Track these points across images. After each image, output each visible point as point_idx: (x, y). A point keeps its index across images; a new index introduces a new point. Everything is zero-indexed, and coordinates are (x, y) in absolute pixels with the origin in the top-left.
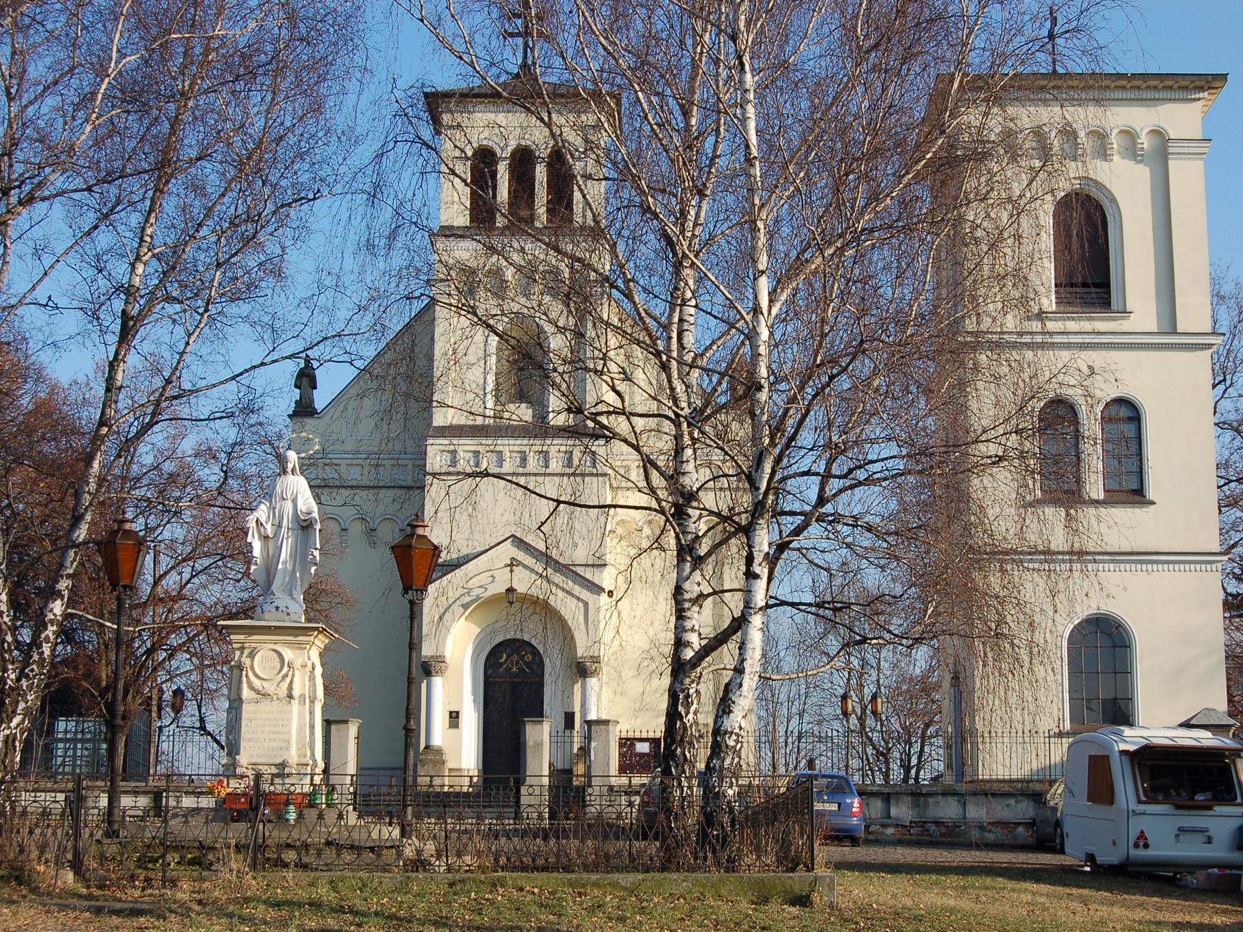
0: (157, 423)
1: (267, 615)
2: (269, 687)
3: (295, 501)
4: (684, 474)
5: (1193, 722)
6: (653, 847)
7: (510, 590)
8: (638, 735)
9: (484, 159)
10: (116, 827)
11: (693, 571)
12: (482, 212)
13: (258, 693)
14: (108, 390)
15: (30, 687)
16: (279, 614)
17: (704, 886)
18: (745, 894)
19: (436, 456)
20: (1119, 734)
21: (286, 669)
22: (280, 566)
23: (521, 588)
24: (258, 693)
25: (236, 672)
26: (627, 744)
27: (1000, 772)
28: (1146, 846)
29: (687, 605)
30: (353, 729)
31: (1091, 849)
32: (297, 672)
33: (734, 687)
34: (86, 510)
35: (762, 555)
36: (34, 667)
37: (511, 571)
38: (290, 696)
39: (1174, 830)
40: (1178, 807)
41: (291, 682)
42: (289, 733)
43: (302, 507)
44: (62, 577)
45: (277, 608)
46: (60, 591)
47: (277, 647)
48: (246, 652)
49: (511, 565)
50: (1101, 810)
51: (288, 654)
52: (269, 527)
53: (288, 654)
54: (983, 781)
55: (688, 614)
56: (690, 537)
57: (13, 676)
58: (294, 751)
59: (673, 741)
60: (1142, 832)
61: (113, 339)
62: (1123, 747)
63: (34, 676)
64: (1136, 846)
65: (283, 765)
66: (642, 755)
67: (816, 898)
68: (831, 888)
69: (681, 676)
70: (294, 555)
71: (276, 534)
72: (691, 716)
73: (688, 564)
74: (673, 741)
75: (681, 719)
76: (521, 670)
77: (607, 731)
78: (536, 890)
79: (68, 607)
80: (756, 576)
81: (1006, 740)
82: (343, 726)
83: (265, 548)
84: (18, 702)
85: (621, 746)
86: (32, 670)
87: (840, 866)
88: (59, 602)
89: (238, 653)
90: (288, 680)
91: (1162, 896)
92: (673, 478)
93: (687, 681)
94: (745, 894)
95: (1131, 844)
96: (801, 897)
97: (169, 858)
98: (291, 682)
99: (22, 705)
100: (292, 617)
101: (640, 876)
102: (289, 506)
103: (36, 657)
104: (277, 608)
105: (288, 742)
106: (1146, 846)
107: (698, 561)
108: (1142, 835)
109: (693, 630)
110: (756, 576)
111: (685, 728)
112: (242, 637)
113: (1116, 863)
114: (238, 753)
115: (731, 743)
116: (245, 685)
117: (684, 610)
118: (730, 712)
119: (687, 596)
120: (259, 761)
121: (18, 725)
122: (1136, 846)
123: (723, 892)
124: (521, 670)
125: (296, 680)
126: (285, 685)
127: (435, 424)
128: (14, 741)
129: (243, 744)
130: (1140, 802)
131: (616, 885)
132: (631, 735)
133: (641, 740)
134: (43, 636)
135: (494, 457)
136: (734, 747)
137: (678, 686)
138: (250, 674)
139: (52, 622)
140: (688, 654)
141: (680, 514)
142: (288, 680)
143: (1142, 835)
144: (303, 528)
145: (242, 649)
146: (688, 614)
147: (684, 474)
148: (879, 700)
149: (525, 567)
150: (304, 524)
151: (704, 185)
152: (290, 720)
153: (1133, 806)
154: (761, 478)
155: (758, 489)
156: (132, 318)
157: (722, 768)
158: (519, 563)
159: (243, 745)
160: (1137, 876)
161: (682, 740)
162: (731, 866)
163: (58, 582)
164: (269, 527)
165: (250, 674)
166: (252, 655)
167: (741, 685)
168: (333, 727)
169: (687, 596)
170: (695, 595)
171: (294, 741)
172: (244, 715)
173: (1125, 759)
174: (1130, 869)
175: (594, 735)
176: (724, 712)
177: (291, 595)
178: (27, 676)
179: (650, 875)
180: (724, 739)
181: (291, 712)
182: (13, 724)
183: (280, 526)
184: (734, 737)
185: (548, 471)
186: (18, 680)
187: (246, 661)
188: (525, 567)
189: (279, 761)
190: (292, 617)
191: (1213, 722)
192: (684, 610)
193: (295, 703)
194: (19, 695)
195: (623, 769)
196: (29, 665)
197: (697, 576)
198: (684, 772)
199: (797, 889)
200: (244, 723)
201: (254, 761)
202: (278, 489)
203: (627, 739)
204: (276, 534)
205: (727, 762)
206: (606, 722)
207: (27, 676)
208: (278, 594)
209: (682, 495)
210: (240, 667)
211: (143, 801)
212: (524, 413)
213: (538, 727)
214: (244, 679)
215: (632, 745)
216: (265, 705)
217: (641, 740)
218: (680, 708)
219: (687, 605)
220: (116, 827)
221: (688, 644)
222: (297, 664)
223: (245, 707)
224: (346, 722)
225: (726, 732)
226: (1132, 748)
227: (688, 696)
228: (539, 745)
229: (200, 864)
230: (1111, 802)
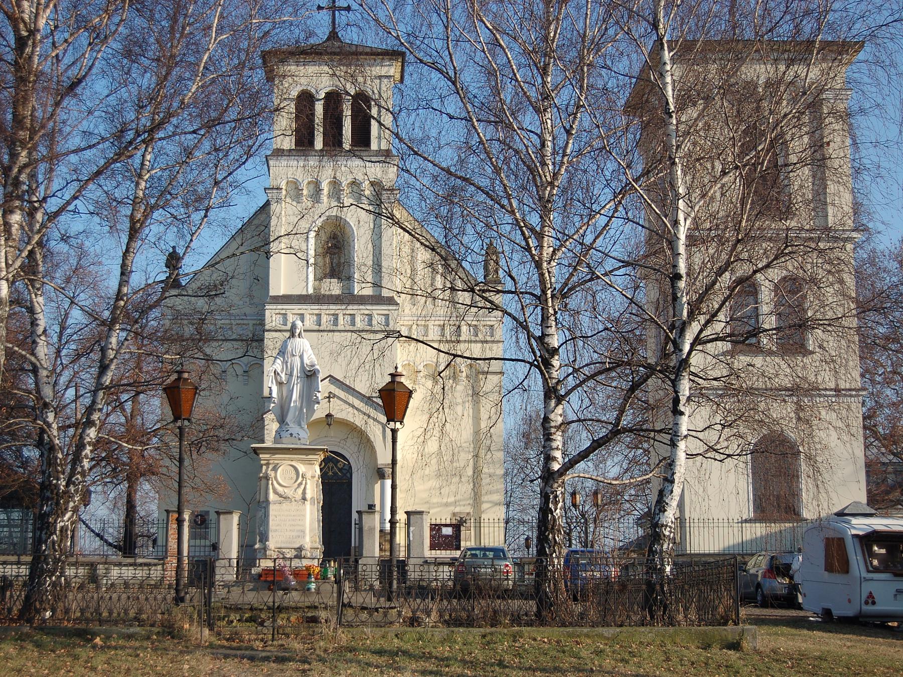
0: (166, 298)
1: (284, 440)
2: (289, 492)
3: (301, 357)
4: (548, 335)
5: (846, 512)
6: (532, 606)
7: (329, 416)
8: (443, 522)
9: (306, 99)
10: (182, 594)
11: (557, 405)
12: (304, 141)
13: (281, 496)
14: (122, 274)
15: (76, 491)
16: (293, 438)
17: (664, 636)
18: (693, 642)
19: (272, 316)
20: (848, 522)
21: (300, 479)
22: (292, 405)
23: (338, 415)
24: (281, 496)
25: (263, 482)
26: (436, 528)
27: (707, 548)
28: (874, 603)
29: (553, 430)
30: (236, 518)
31: (827, 605)
32: (308, 481)
33: (666, 492)
34: (112, 360)
35: (685, 398)
36: (79, 476)
37: (329, 402)
38: (304, 499)
39: (893, 592)
40: (896, 575)
41: (305, 489)
42: (304, 525)
43: (307, 361)
44: (95, 410)
45: (291, 435)
46: (94, 421)
47: (293, 463)
48: (271, 467)
49: (329, 397)
50: (838, 578)
51: (302, 468)
52: (283, 375)
53: (302, 468)
54: (691, 554)
55: (553, 437)
56: (554, 381)
57: (64, 483)
58: (308, 539)
59: (546, 529)
60: (871, 593)
61: (125, 239)
62: (854, 532)
63: (79, 483)
64: (867, 603)
65: (300, 549)
66: (447, 536)
67: (745, 644)
68: (754, 637)
69: (551, 482)
70: (301, 396)
71: (289, 381)
72: (558, 511)
73: (553, 401)
74: (546, 529)
75: (552, 514)
76: (335, 474)
77: (422, 519)
78: (546, 640)
79: (99, 433)
80: (682, 413)
81: (721, 525)
82: (229, 516)
83: (280, 391)
84: (69, 502)
85: (431, 530)
86: (77, 479)
87: (759, 621)
88: (93, 429)
89: (264, 468)
90: (303, 487)
91: (866, 636)
92: (541, 339)
93: (556, 485)
94: (693, 642)
95: (863, 602)
96: (733, 644)
97: (232, 617)
98: (305, 489)
99: (71, 504)
100: (302, 441)
101: (618, 630)
102: (297, 361)
103: (79, 469)
104: (291, 435)
105: (303, 532)
106: (874, 603)
107: (560, 400)
108: (870, 596)
109: (557, 449)
110: (682, 413)
111: (555, 520)
112: (268, 456)
113: (851, 615)
114: (267, 540)
115: (667, 533)
116: (271, 491)
117: (551, 434)
118: (665, 510)
119: (553, 424)
120: (283, 546)
121: (69, 519)
122: (867, 603)
123: (678, 641)
124: (335, 474)
125: (308, 486)
126: (300, 491)
127: (271, 294)
128: (66, 531)
129: (271, 534)
130: (869, 571)
131: (601, 636)
132: (438, 522)
133: (446, 525)
134: (84, 453)
135: (348, 318)
136: (669, 536)
137: (548, 490)
138: (275, 483)
139: (89, 443)
140: (556, 467)
141: (544, 364)
142: (303, 487)
143: (870, 596)
144: (308, 376)
145: (268, 464)
146: (553, 437)
147: (548, 335)
148: (599, 496)
149: (339, 398)
150: (309, 374)
151: (571, 126)
152: (304, 516)
153: (864, 574)
154: (683, 342)
155: (681, 350)
156: (138, 221)
157: (661, 551)
158: (335, 396)
159: (271, 535)
160: (865, 624)
161: (553, 528)
162: (672, 622)
163: (92, 414)
164: (283, 375)
165: (275, 483)
166: (275, 469)
167: (672, 492)
168: (222, 516)
169: (553, 424)
170: (559, 423)
171: (307, 531)
172: (271, 513)
173: (856, 541)
174: (861, 619)
175: (412, 522)
176: (660, 511)
177: (300, 425)
178: (74, 483)
179: (624, 629)
180: (661, 530)
181: (305, 510)
182: (66, 518)
183: (291, 375)
184: (668, 529)
185: (322, 328)
186: (67, 485)
187: (271, 474)
188: (339, 398)
189: (297, 546)
190: (302, 441)
191: (860, 512)
192: (551, 434)
193: (308, 503)
194: (70, 497)
195: (433, 547)
196: (74, 475)
197: (559, 410)
198: (555, 551)
199: (730, 638)
200: (271, 518)
201: (279, 546)
202: (289, 348)
203: (436, 525)
204: (289, 381)
205: (665, 547)
206: (421, 513)
207: (74, 483)
208: (291, 425)
209: (548, 351)
210: (267, 478)
211: (82, 571)
212: (334, 287)
213: (371, 516)
214: (271, 487)
215: (440, 529)
216: (286, 506)
217: (446, 525)
218: (551, 505)
219: (553, 430)
220: (182, 594)
221: (554, 459)
222: (309, 475)
223: (272, 507)
224: (231, 513)
225: (663, 525)
226: (861, 533)
227: (556, 496)
228: (372, 529)
229: (255, 621)
230: (847, 572)
